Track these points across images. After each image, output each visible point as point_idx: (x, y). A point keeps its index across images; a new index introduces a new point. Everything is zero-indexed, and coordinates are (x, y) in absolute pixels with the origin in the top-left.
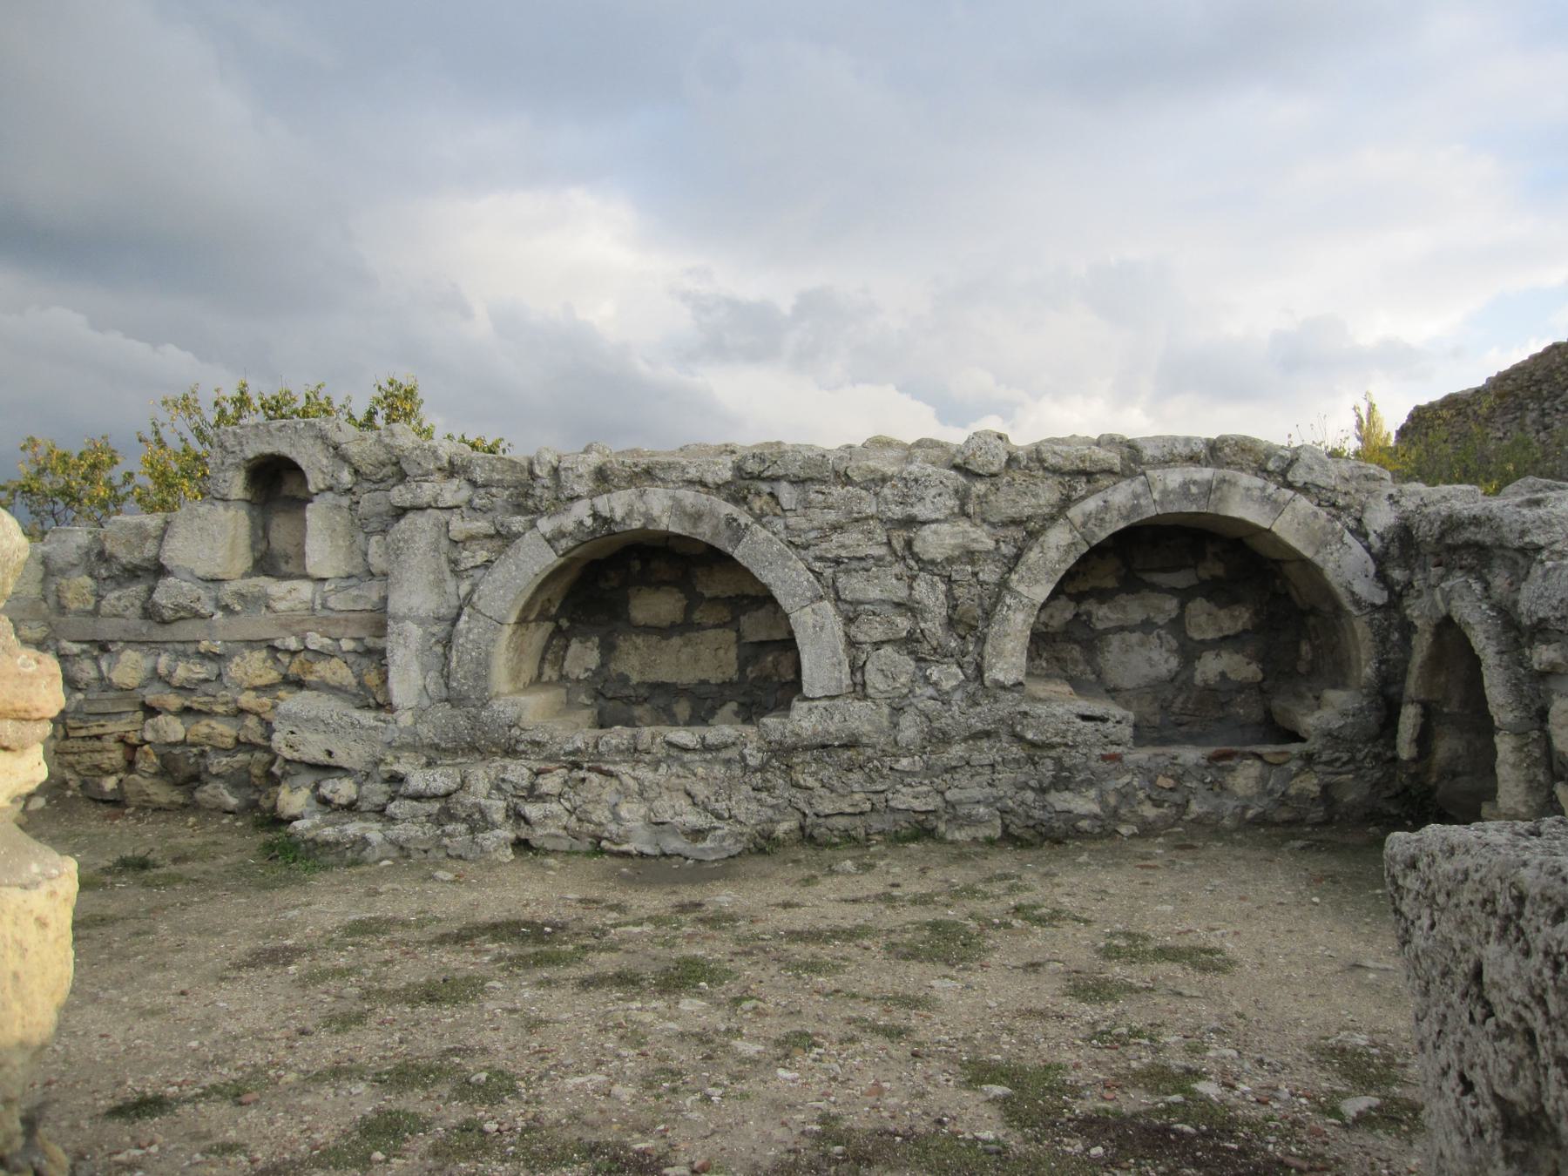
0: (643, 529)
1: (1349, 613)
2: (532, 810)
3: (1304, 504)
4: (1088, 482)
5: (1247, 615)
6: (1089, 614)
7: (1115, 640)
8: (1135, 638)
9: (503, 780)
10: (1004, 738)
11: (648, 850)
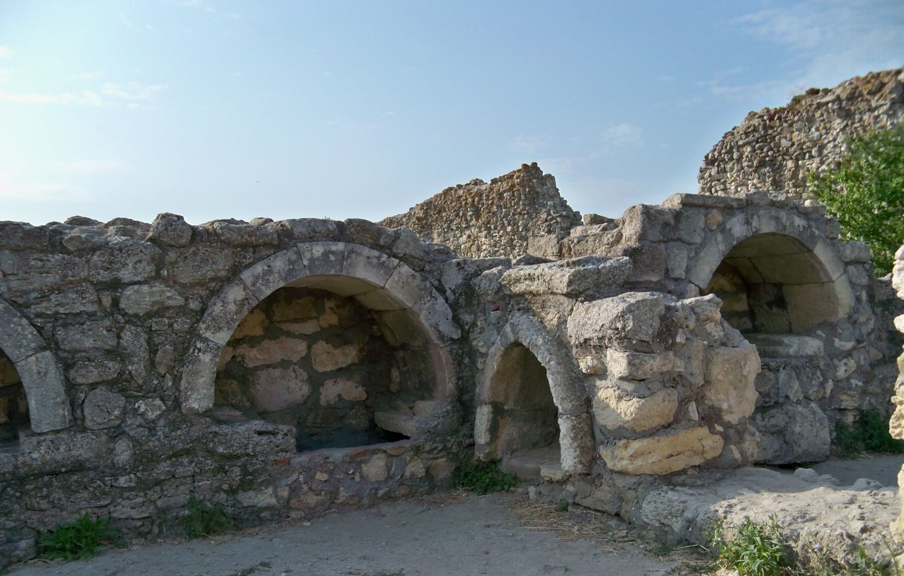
1: (436, 345)
3: (405, 269)
4: (254, 252)
5: (354, 353)
6: (243, 357)
7: (263, 375)
8: (277, 372)
10: (200, 453)
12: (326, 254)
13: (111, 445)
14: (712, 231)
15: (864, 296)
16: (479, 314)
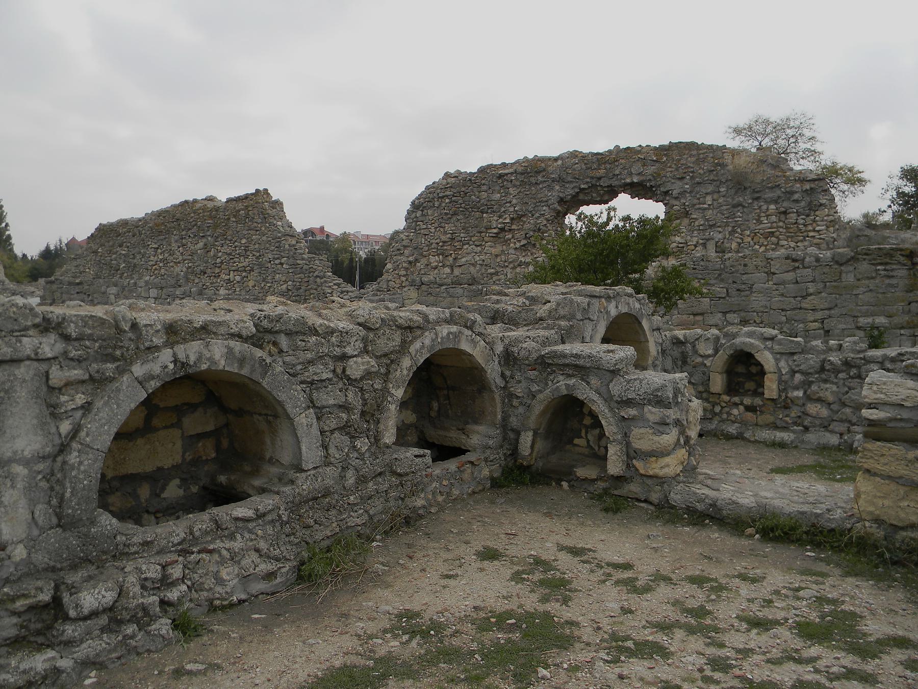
0: (208, 371)
2: (173, 595)
9: (146, 579)
11: (243, 596)
12: (448, 334)
13: (343, 474)
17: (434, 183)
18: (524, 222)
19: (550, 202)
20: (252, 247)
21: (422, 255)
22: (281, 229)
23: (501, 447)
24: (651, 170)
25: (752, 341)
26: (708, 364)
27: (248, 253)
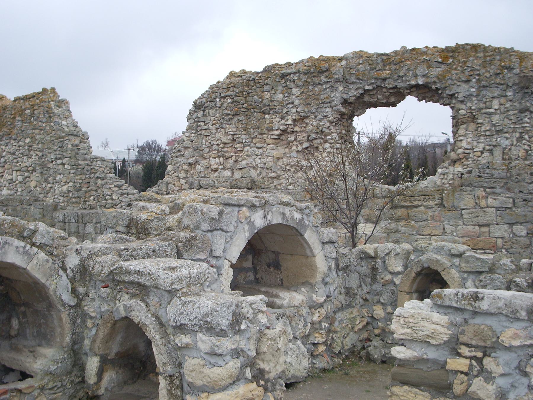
3: (42, 255)
14: (242, 223)
15: (333, 266)
16: (91, 288)
17: (218, 82)
18: (307, 124)
19: (333, 103)
20: (35, 146)
21: (202, 156)
22: (66, 129)
23: (70, 373)
24: (436, 71)
25: (439, 257)
26: (397, 282)
27: (31, 153)
